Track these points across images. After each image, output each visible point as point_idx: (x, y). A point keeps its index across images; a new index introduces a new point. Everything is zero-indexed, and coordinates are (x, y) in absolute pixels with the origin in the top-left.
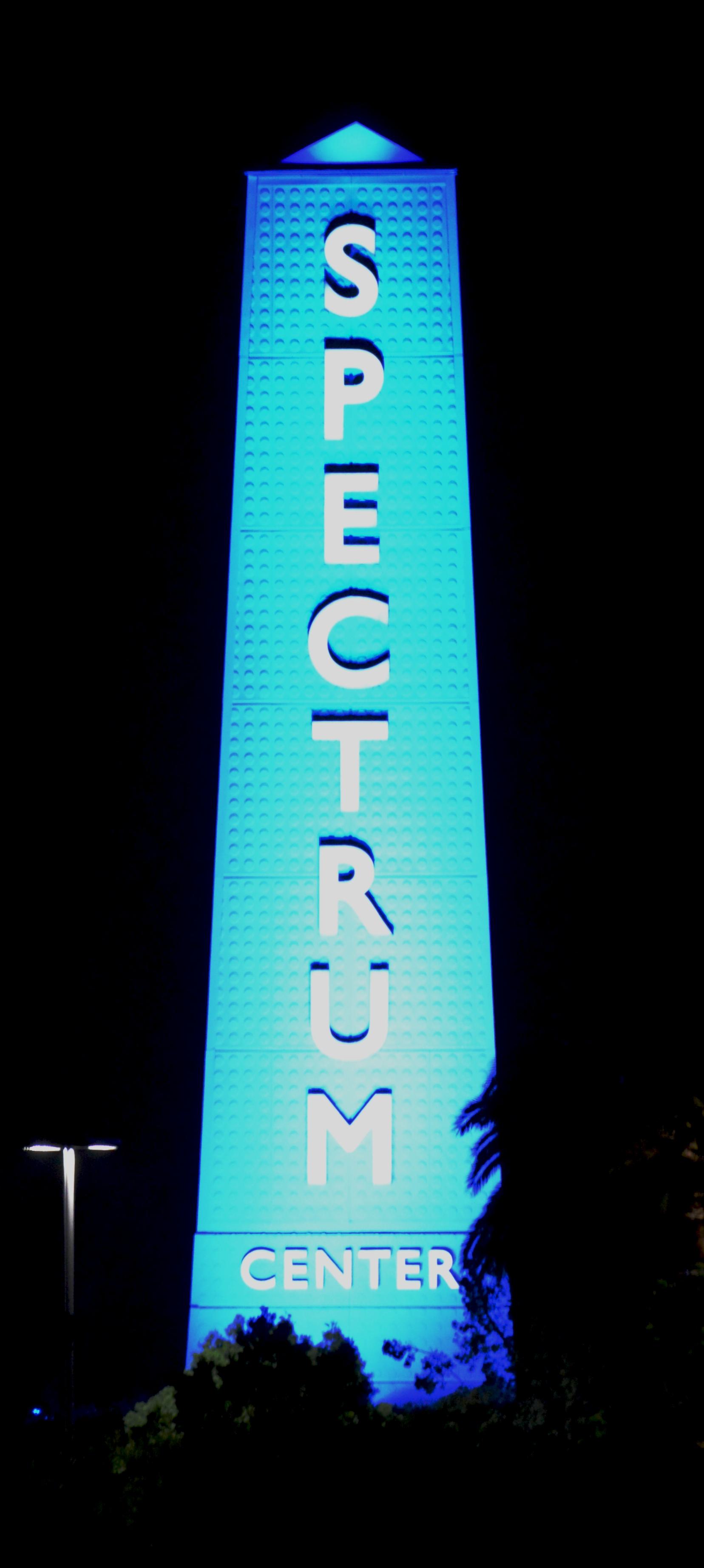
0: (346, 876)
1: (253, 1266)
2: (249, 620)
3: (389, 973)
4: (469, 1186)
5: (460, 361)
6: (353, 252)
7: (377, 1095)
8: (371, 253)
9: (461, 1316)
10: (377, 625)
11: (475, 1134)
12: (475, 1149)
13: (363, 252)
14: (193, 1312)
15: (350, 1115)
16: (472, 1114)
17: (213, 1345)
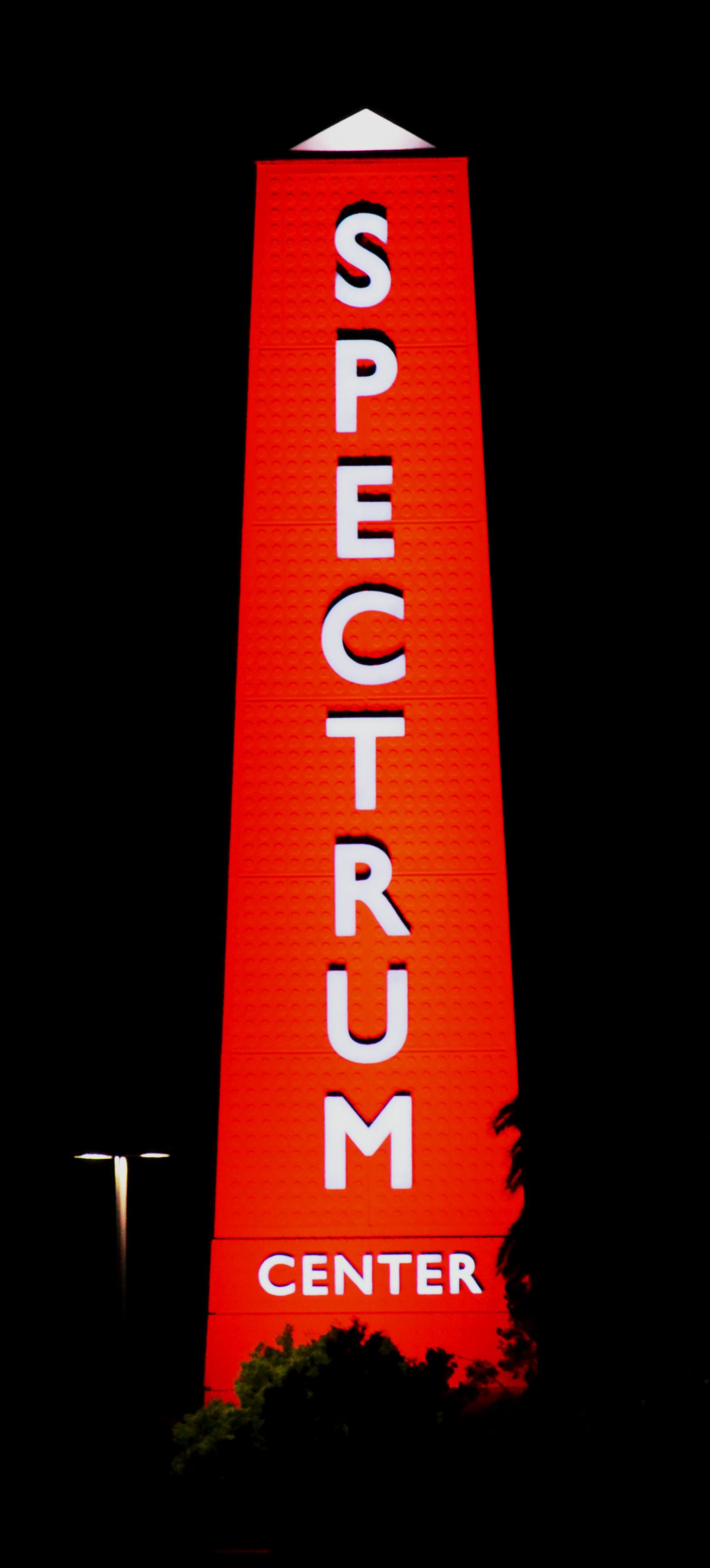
9: (506, 1324)
10: (393, 619)
16: (507, 1116)
17: (262, 1354)
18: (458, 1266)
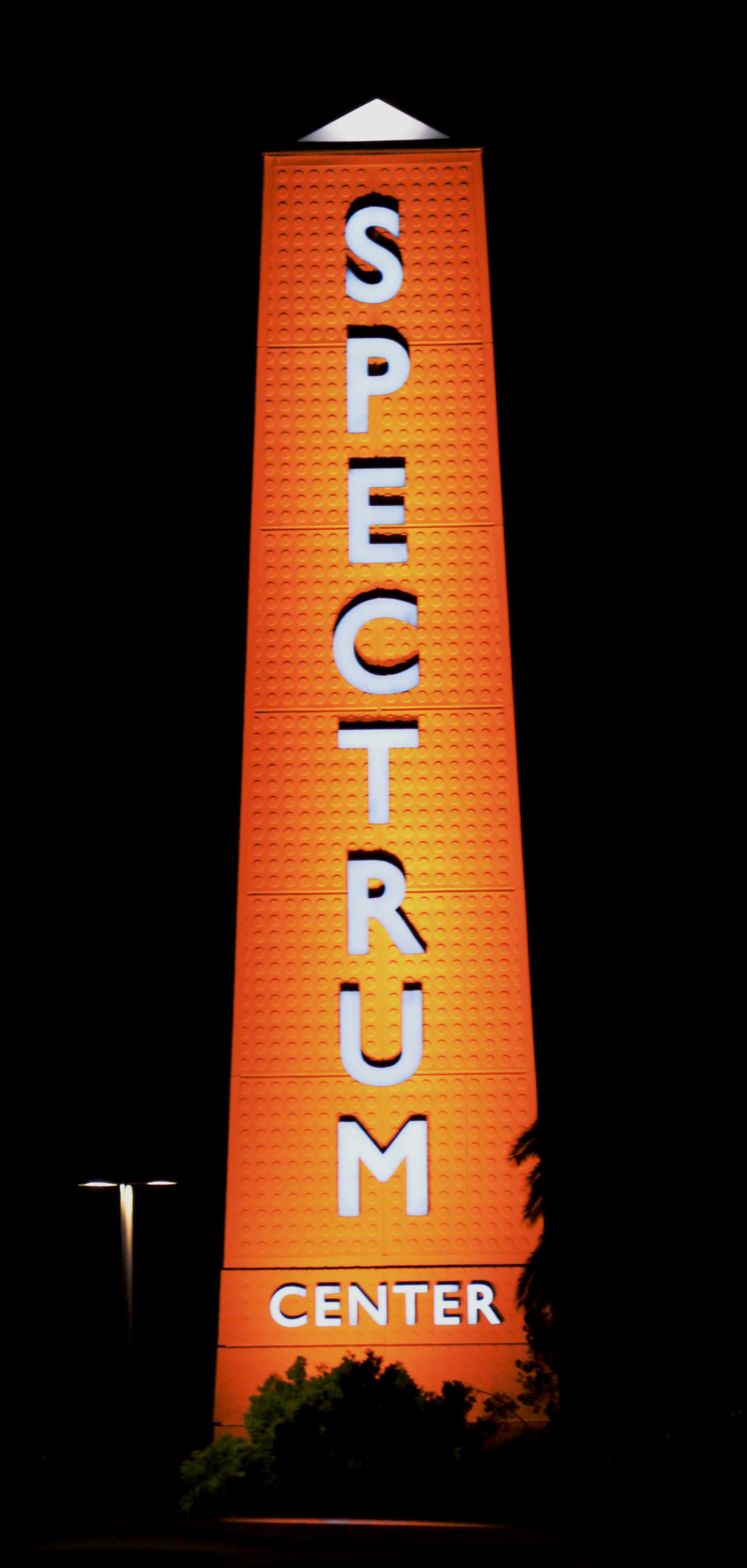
0: (376, 892)
1: (284, 1303)
3: (423, 993)
4: (526, 1216)
5: (489, 348)
6: (376, 234)
7: (412, 1124)
8: (394, 236)
9: (524, 1354)
11: (532, 1163)
12: (531, 1178)
13: (385, 235)
14: (220, 1351)
17: (273, 1387)
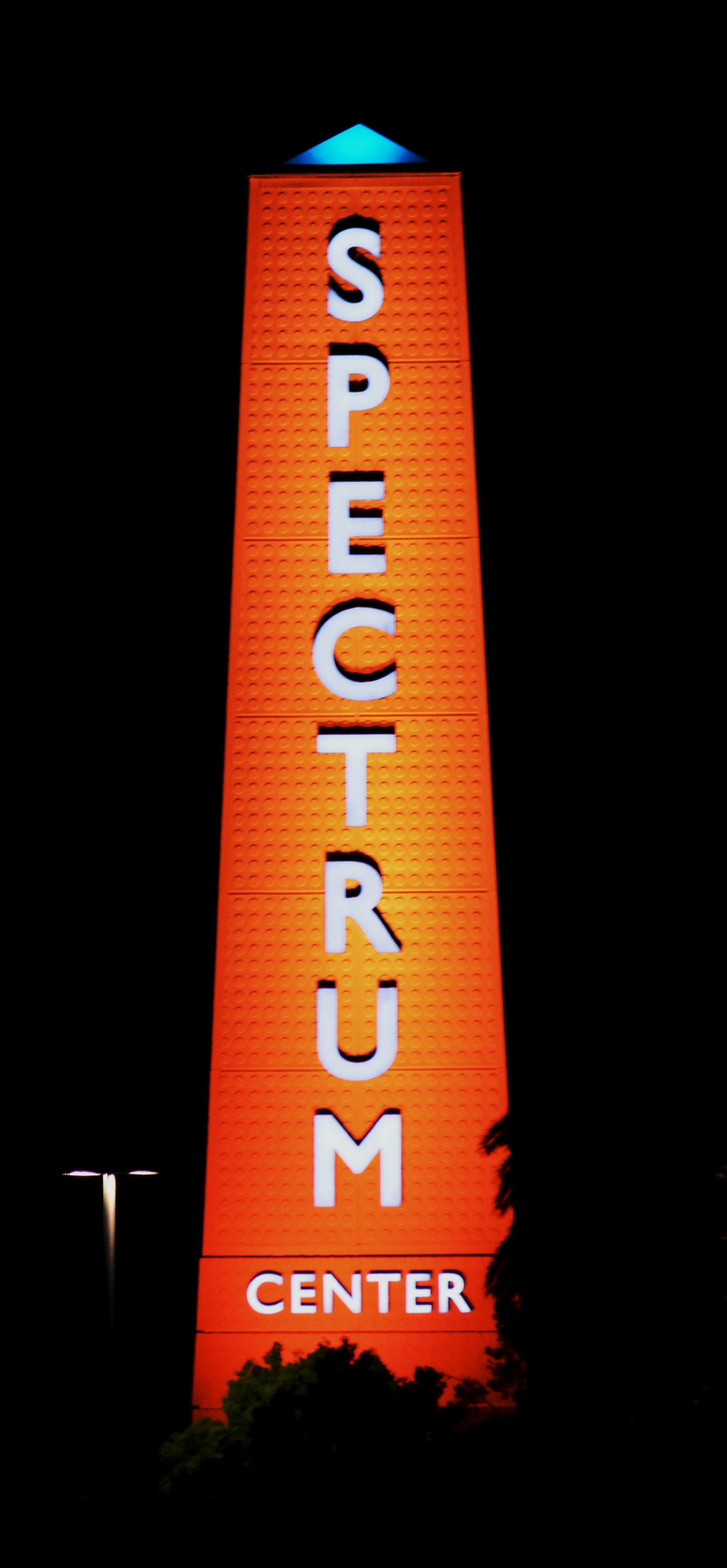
0: (353, 892)
2: (253, 631)
4: (497, 1207)
5: (467, 366)
8: (374, 257)
11: (501, 1154)
13: (367, 256)
14: (199, 1336)
15: (358, 1135)
17: (250, 1372)
18: (447, 1285)
